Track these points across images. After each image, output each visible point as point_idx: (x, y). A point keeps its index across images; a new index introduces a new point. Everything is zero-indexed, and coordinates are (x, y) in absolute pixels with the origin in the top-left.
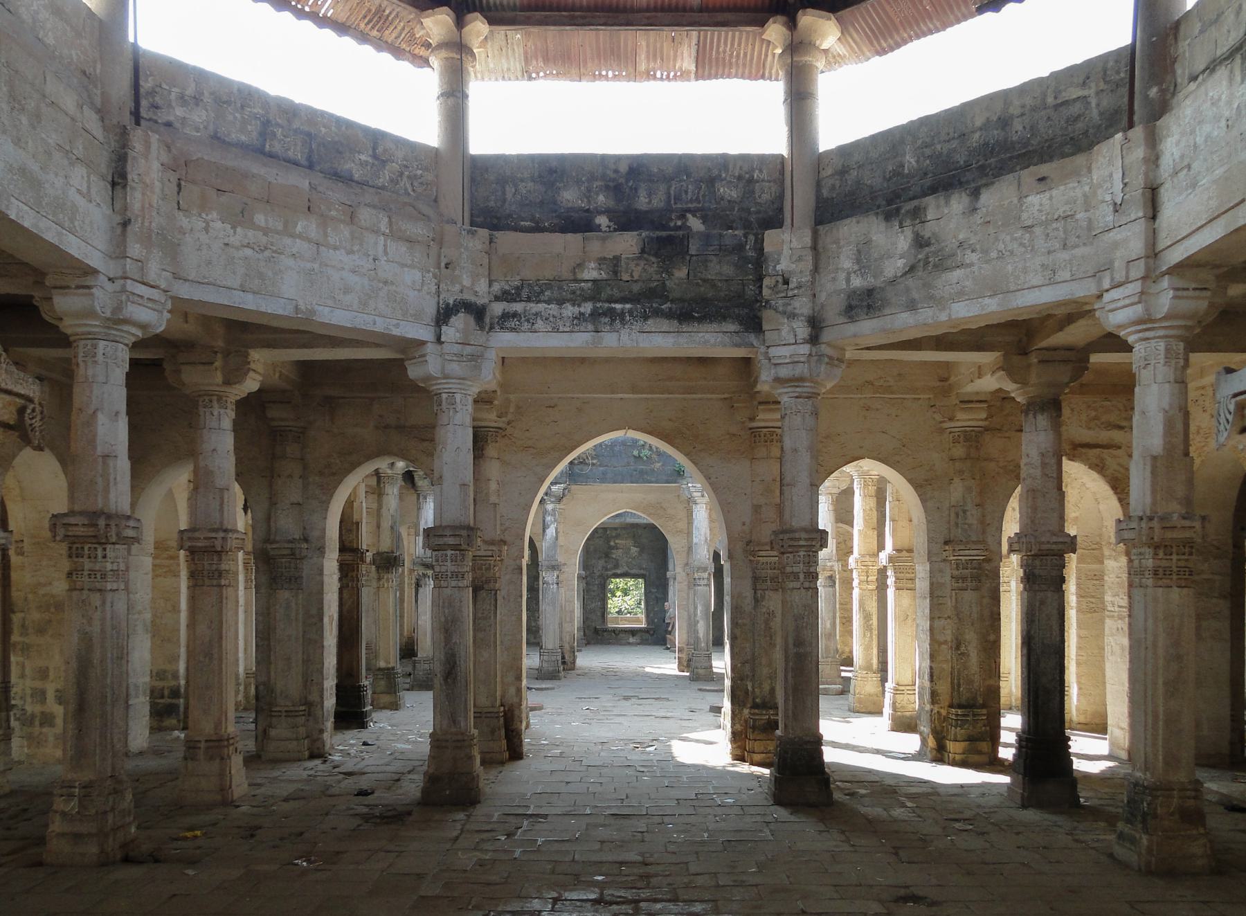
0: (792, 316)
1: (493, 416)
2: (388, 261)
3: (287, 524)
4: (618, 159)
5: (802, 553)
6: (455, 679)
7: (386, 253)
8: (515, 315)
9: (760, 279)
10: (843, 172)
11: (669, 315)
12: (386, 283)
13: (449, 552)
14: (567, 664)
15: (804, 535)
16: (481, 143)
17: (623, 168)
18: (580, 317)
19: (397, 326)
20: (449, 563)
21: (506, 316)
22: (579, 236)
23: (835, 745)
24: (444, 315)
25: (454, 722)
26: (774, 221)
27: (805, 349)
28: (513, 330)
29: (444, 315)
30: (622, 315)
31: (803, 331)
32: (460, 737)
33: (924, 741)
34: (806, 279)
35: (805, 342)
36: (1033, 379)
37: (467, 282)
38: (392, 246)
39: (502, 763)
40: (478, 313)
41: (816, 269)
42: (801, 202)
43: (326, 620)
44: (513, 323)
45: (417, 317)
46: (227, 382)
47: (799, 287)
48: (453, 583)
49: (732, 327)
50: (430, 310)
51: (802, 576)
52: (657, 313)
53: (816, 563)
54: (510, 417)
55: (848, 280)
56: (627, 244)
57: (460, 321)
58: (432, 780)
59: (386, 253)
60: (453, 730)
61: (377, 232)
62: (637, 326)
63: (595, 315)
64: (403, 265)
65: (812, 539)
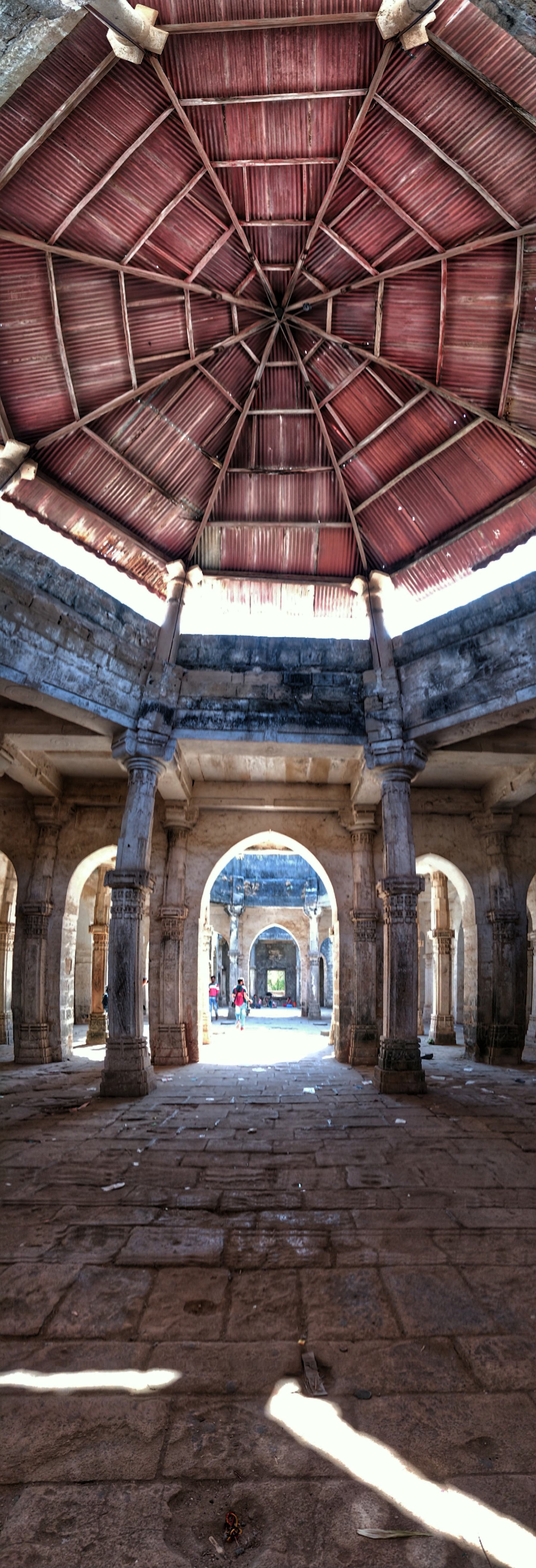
0: (388, 721)
1: (183, 818)
2: (108, 670)
4: (269, 639)
5: (404, 895)
6: (125, 994)
7: (108, 664)
8: (194, 718)
9: (361, 702)
10: (408, 644)
11: (300, 722)
12: (103, 682)
13: (125, 890)
15: (406, 880)
16: (187, 627)
17: (271, 643)
18: (238, 722)
19: (105, 711)
20: (124, 899)
21: (188, 718)
22: (241, 674)
24: (144, 710)
25: (125, 1028)
26: (370, 667)
27: (398, 743)
28: (192, 728)
29: (144, 710)
30: (267, 720)
31: (395, 731)
32: (129, 1041)
34: (395, 696)
35: (398, 738)
37: (163, 692)
38: (113, 662)
40: (168, 714)
41: (401, 692)
42: (385, 656)
45: (123, 709)
47: (391, 702)
48: (126, 915)
49: (343, 731)
50: (133, 705)
51: (404, 913)
52: (292, 721)
53: (416, 904)
54: (194, 821)
55: (426, 693)
56: (273, 678)
57: (153, 716)
59: (108, 664)
60: (124, 1035)
61: (105, 651)
62: (276, 729)
63: (248, 720)
64: (120, 676)
65: (412, 883)
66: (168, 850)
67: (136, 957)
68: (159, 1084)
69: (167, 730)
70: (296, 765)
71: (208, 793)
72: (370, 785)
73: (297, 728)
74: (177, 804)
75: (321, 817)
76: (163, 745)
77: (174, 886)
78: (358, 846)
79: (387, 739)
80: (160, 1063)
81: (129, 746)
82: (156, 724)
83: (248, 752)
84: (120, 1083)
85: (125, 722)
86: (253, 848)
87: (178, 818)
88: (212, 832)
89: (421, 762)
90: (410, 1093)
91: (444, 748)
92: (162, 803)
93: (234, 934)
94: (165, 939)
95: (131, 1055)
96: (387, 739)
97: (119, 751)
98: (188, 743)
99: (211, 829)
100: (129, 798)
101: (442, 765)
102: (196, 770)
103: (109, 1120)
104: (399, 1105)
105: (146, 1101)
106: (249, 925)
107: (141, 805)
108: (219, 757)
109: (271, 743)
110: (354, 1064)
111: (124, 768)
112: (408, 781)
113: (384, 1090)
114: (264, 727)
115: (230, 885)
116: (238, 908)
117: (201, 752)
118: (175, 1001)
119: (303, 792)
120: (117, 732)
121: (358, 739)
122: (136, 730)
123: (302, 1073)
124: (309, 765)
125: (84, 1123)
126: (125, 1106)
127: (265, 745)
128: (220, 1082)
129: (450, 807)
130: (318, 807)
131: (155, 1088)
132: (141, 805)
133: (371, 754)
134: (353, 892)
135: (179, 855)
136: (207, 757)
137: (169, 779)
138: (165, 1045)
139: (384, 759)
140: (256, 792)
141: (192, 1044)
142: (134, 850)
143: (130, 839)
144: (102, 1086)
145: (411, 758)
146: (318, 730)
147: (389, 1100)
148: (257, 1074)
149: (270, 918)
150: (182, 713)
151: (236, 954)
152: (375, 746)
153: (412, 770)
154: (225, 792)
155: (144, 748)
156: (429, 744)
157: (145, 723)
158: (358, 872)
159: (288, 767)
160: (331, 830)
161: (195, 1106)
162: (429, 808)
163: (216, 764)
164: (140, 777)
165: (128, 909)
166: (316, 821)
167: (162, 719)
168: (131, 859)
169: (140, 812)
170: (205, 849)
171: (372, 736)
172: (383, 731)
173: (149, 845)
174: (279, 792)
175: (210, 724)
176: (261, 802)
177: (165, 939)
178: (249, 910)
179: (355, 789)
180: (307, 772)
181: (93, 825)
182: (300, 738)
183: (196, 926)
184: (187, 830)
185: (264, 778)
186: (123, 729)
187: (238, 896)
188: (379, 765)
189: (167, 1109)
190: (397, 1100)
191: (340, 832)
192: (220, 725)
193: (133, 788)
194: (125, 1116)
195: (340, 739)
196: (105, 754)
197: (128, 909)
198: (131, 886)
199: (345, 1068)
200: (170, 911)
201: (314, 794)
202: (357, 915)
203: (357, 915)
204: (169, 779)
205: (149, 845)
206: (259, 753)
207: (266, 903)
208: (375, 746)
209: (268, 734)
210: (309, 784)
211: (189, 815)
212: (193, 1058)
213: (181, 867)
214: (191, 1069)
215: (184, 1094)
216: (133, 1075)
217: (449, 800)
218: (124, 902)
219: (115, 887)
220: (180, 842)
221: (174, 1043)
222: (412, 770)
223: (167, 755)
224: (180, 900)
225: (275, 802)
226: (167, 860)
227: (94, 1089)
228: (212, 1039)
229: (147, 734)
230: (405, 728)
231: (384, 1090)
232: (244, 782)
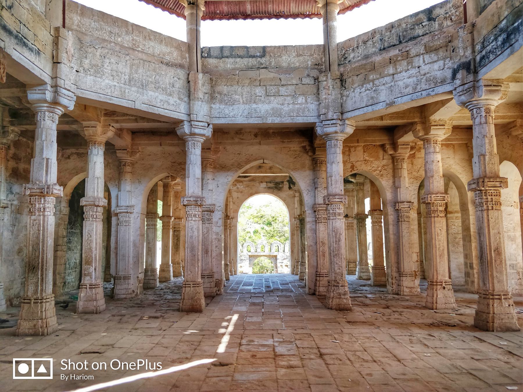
21: (483, 58)
28: (485, 66)
82: (463, 79)
150: (478, 58)
229: (461, 88)
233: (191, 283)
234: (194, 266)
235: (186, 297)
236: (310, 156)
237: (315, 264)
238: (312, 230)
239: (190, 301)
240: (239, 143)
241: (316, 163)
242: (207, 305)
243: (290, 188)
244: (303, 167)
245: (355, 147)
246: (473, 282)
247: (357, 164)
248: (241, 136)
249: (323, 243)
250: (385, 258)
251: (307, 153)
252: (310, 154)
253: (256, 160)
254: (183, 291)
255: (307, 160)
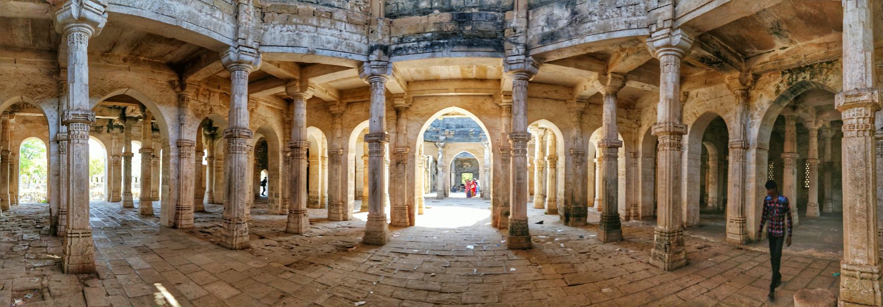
1: (403, 102)
3: (338, 144)
8: (400, 49)
14: (446, 195)
18: (426, 47)
21: (397, 49)
23: (765, 253)
24: (371, 50)
25: (376, 210)
27: (523, 57)
28: (400, 55)
29: (371, 50)
31: (522, 50)
33: (561, 218)
36: (609, 83)
39: (406, 227)
43: (349, 175)
44: (399, 52)
45: (359, 52)
46: (302, 91)
50: (365, 48)
57: (377, 52)
58: (367, 233)
66: (397, 120)
67: (381, 175)
68: (392, 238)
69: (386, 58)
70: (467, 69)
71: (417, 89)
72: (509, 81)
73: (462, 49)
74: (400, 96)
75: (483, 98)
76: (385, 67)
77: (401, 138)
78: (504, 114)
79: (516, 52)
80: (393, 226)
81: (367, 71)
82: (379, 57)
83: (434, 64)
84: (373, 239)
85: (362, 58)
86: (447, 114)
87: (401, 103)
88: (421, 108)
89: (535, 69)
90: (524, 249)
91: (549, 62)
92: (390, 96)
93: (440, 156)
94: (398, 163)
95: (378, 224)
96: (516, 52)
97: (362, 74)
98: (399, 63)
99: (420, 107)
100: (372, 98)
101: (548, 71)
102: (409, 77)
103: (363, 259)
104: (515, 258)
105: (383, 248)
106: (449, 152)
107: (378, 101)
108: (420, 69)
109: (447, 58)
110: (500, 228)
111: (367, 83)
112: (527, 80)
113: (511, 247)
114: (442, 49)
115: (438, 132)
116: (442, 144)
117: (407, 67)
118: (403, 194)
119: (472, 84)
120: (360, 64)
121: (500, 54)
122: (369, 62)
123: (466, 235)
124: (474, 69)
125: (353, 259)
126: (373, 251)
127: (444, 59)
128: (423, 239)
129: (556, 96)
130: (482, 92)
131: (389, 241)
132: (378, 101)
133: (507, 63)
134: (500, 138)
135: (403, 122)
136: (413, 69)
137: (392, 84)
138: (397, 216)
139: (514, 67)
140: (444, 85)
141: (411, 216)
142: (377, 123)
143: (375, 118)
144: (364, 238)
145: (529, 67)
146: (475, 49)
147: (511, 254)
148: (445, 234)
149: (459, 149)
150: (393, 47)
151: (441, 166)
152: (510, 58)
153: (530, 73)
154: (426, 86)
155: (375, 71)
156: (541, 59)
157: (373, 57)
158: (504, 127)
159: (462, 70)
160: (489, 105)
161: (407, 254)
162: (545, 95)
163: (419, 72)
164: (376, 86)
165: (377, 152)
166: (481, 100)
167: (382, 53)
168: (376, 128)
169: (379, 102)
170: (417, 118)
171: (508, 52)
172: (514, 49)
173: (384, 120)
174: (458, 85)
175: (410, 51)
176: (447, 90)
177: (398, 163)
178: (449, 144)
179: (502, 82)
180: (473, 73)
181: (358, 111)
182: (464, 54)
183: (414, 157)
184: (407, 108)
185: (448, 77)
186: (362, 63)
187: (442, 138)
188: (511, 70)
189: (393, 255)
190: (516, 254)
191: (495, 107)
192: (416, 51)
193: (373, 92)
194: (372, 258)
195: (489, 54)
196: (356, 77)
197: (377, 152)
198: (377, 141)
199: (494, 230)
200: (400, 150)
201: (479, 85)
202: (502, 150)
203: (502, 150)
204: (392, 84)
205: (384, 120)
206: (441, 64)
207: (458, 141)
208: (510, 58)
209: (444, 52)
210: (475, 80)
211: (407, 100)
212: (412, 223)
213: (404, 128)
214: (410, 229)
215: (402, 246)
216: (379, 234)
217: (556, 91)
218: (375, 149)
219: (370, 142)
220: (403, 115)
221: (402, 215)
222: (530, 73)
223: (388, 72)
224: (405, 144)
225: (456, 90)
226: (397, 125)
227: (360, 238)
228: (424, 210)
229: (376, 63)
230: (527, 48)
231: (511, 247)
232: (437, 80)
233: (80, 232)
234: (83, 207)
235: (73, 252)
236: (177, 92)
237: (176, 197)
238: (175, 164)
239: (80, 257)
240: (105, 66)
241: (183, 100)
242: (800, 223)
243: (108, 131)
244: (169, 102)
245: (215, 92)
246: (277, 207)
247: (215, 108)
248: (108, 59)
249: (186, 178)
250: (640, 172)
251: (174, 88)
252: (178, 89)
253: (121, 88)
254: (69, 244)
255: (172, 95)
